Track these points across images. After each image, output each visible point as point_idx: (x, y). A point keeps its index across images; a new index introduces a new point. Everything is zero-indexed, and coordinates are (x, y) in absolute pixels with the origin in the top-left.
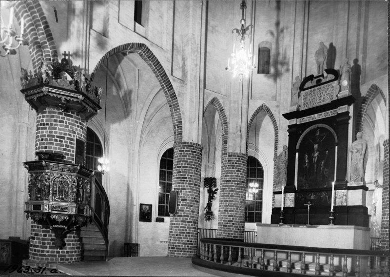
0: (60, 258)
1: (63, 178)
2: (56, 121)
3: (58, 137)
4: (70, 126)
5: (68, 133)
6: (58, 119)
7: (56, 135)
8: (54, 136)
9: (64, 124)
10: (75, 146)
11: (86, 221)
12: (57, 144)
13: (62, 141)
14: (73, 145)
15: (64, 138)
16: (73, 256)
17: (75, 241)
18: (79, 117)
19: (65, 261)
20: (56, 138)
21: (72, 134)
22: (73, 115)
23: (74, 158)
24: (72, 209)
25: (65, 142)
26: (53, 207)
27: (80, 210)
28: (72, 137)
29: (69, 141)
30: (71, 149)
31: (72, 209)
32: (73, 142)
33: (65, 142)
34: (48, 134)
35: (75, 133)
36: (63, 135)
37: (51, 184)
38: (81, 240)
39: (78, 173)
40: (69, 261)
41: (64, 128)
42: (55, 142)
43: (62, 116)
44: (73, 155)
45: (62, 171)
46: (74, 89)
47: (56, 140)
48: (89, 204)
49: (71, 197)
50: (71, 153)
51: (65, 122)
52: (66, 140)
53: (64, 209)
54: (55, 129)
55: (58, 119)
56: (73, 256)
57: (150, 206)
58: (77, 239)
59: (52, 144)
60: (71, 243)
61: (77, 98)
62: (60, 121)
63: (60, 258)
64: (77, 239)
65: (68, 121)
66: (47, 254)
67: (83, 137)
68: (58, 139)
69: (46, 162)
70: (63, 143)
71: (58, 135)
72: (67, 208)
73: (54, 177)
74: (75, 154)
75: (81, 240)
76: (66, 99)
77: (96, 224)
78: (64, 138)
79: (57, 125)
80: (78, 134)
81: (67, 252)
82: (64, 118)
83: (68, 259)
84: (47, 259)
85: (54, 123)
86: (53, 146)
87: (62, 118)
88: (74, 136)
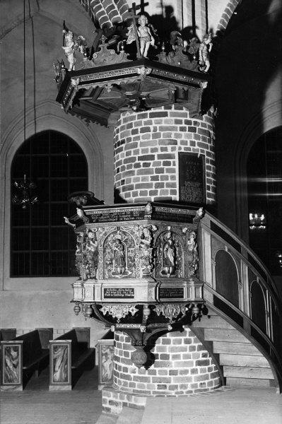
0: (156, 384)
1: (124, 233)
2: (135, 132)
3: (140, 158)
4: (162, 133)
5: (159, 147)
6: (139, 128)
7: (137, 156)
8: (133, 159)
9: (151, 133)
10: (177, 168)
11: (189, 313)
12: (140, 173)
13: (149, 164)
14: (172, 167)
15: (152, 157)
16: (189, 379)
17: (193, 349)
18: (184, 111)
19: (167, 390)
20: (137, 162)
21: (169, 147)
22: (169, 111)
23: (177, 189)
24: (143, 292)
25: (155, 164)
26: (105, 290)
27: (169, 294)
28: (169, 152)
29: (162, 161)
30: (169, 175)
31: (143, 292)
32: (171, 160)
33: (155, 164)
34: (126, 157)
35: (175, 143)
36: (150, 153)
37: (101, 248)
38: (208, 346)
39: (152, 218)
40: (179, 390)
41: (151, 139)
42: (136, 170)
43: (145, 120)
44: (173, 185)
45: (118, 221)
46: (126, 60)
47: (137, 166)
48: (198, 276)
49: (142, 268)
50: (170, 181)
51: (152, 129)
52: (156, 160)
53: (128, 293)
54: (135, 145)
55: (139, 128)
56: (189, 379)
57: (133, 297)
58: (196, 345)
59: (132, 173)
60: (182, 354)
61: (137, 75)
62: (143, 130)
63: (156, 384)
64: (196, 345)
65: (158, 126)
66: (132, 375)
67: (197, 147)
68: (142, 162)
69: (82, 209)
70: (151, 167)
71: (141, 155)
72: (133, 290)
73: (105, 234)
74: (177, 181)
75: (208, 346)
76: (114, 85)
77: (219, 315)
78: (152, 157)
79: (138, 138)
80: (183, 143)
81: (173, 373)
82: (150, 123)
83: (176, 387)
84: (132, 385)
85: (132, 136)
86: (132, 177)
87: (146, 123)
88: (173, 149)
